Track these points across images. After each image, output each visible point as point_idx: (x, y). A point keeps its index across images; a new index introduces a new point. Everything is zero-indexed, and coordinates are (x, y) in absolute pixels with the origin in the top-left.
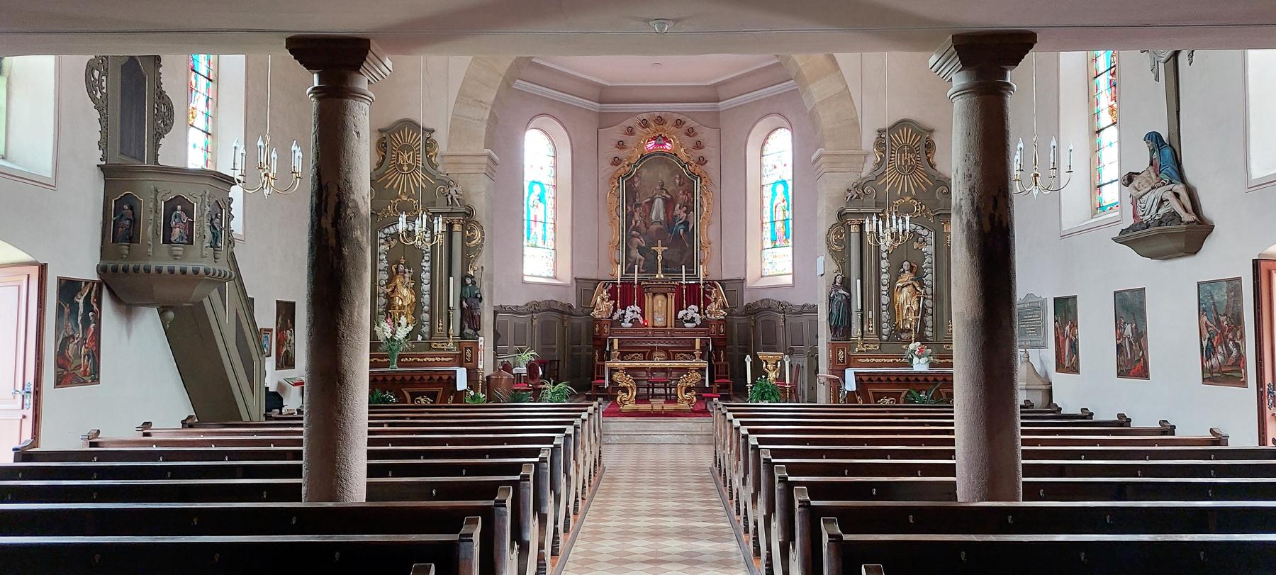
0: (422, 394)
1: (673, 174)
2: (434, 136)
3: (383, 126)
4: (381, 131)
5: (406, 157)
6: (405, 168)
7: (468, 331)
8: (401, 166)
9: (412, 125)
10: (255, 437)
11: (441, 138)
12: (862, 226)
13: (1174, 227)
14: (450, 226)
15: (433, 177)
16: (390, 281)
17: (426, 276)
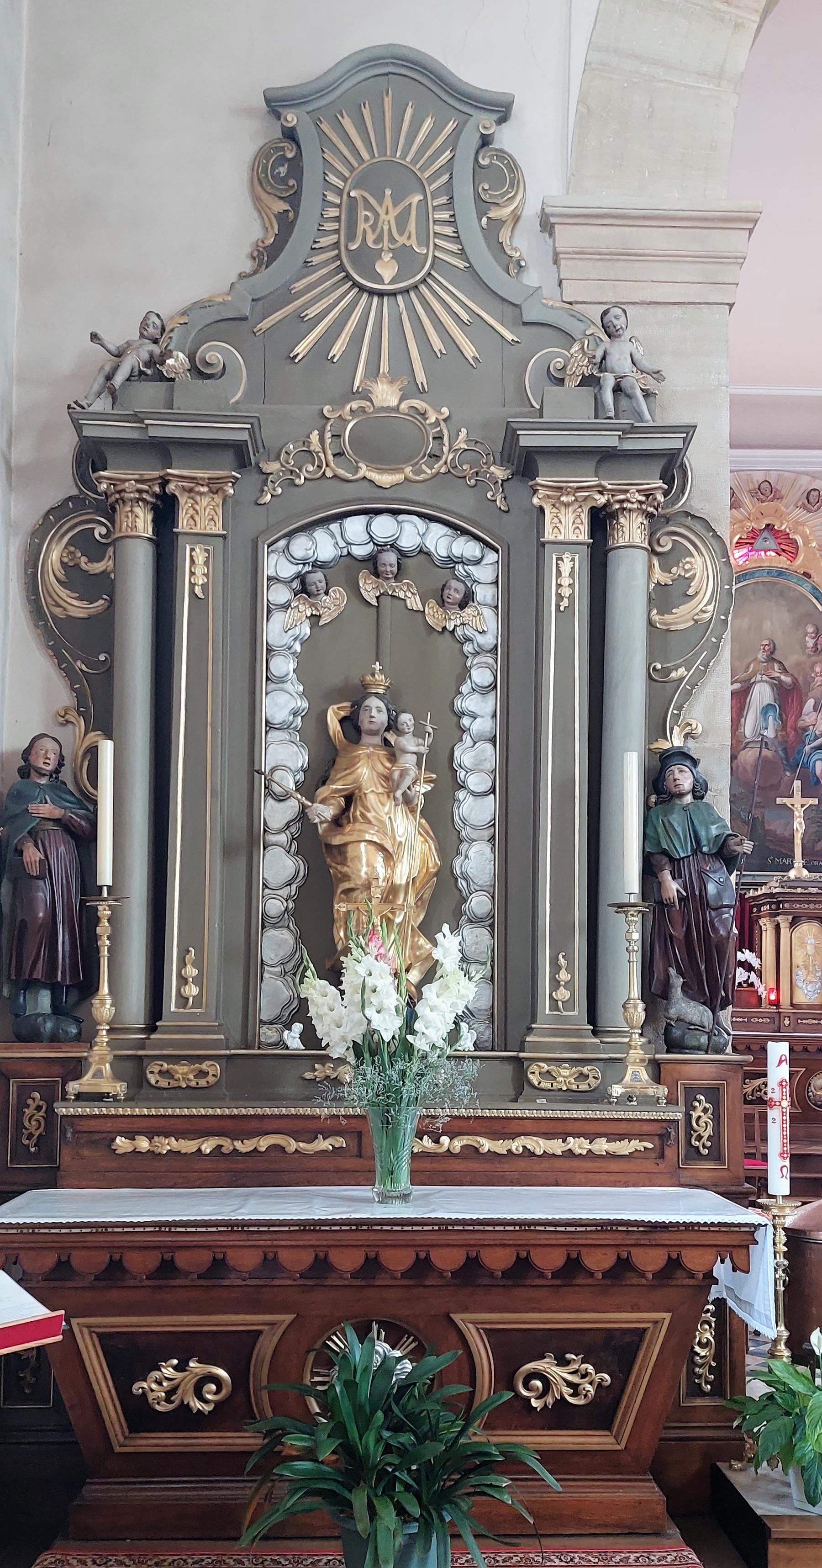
0: (560, 1344)
1: (800, 622)
2: (507, 138)
3: (288, 75)
4: (276, 104)
5: (388, 217)
6: (387, 269)
7: (687, 1009)
8: (366, 259)
9: (409, 74)
10: (162, 1486)
11: (537, 143)
12: (165, 510)
13: (425, 1514)
14: (601, 521)
15: (512, 311)
16: (315, 779)
17: (476, 760)
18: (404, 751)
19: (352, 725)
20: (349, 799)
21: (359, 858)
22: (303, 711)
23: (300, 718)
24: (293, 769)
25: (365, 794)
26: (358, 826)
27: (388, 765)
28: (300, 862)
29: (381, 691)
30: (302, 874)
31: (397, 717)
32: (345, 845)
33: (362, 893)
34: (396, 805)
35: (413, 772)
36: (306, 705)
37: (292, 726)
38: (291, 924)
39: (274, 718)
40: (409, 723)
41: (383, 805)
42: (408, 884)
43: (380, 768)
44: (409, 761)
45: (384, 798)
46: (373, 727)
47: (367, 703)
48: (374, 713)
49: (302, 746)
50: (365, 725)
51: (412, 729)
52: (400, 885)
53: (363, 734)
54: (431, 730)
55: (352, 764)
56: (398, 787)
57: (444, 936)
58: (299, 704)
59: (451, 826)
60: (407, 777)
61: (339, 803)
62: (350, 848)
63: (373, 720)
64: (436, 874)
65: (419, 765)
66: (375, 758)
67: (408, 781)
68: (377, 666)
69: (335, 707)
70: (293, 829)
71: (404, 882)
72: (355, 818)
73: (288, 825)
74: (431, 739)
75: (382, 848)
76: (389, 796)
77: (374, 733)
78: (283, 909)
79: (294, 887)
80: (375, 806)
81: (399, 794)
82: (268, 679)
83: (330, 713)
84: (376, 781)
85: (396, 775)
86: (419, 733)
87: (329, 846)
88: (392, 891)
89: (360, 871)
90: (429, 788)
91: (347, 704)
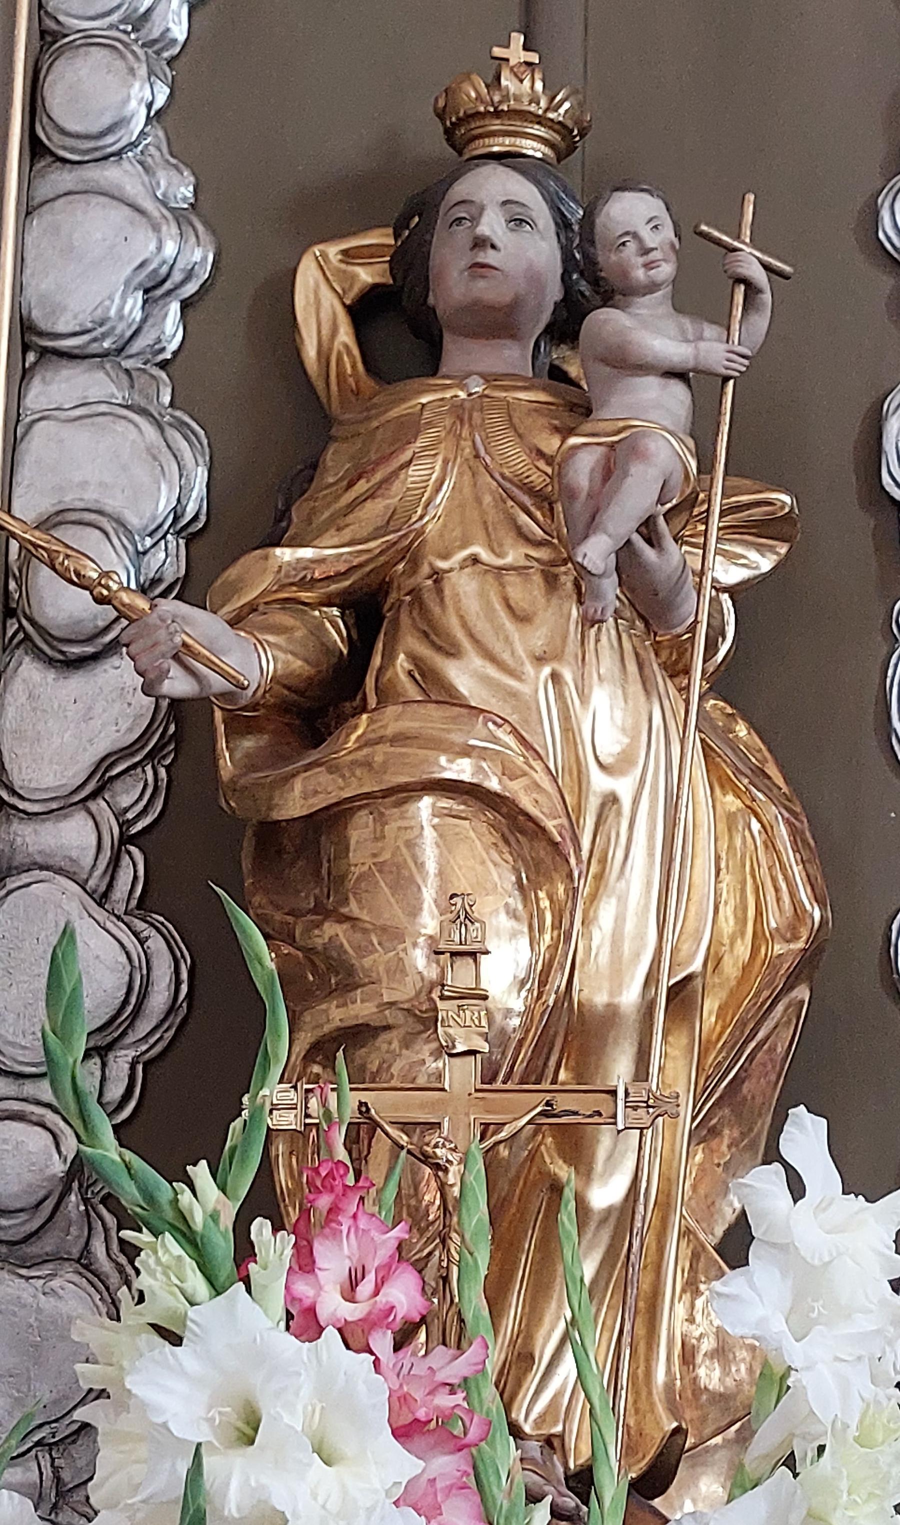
18: (627, 364)
19: (402, 324)
20: (369, 606)
21: (404, 881)
22: (189, 275)
23: (174, 308)
24: (134, 521)
25: (437, 576)
26: (393, 719)
27: (551, 444)
28: (157, 943)
29: (533, 149)
30: (159, 999)
31: (589, 220)
32: (331, 820)
33: (407, 1044)
34: (590, 621)
35: (667, 453)
36: (200, 255)
37: (137, 346)
38: (98, 1247)
39: (56, 310)
40: (651, 239)
41: (522, 618)
42: (648, 1010)
43: (515, 458)
44: (656, 410)
45: (527, 592)
46: (487, 290)
47: (461, 189)
48: (492, 224)
49: (180, 426)
50: (452, 285)
51: (666, 271)
52: (612, 1013)
53: (447, 338)
54: (760, 276)
55: (377, 460)
56: (592, 524)
57: (797, 1187)
58: (170, 249)
59: (873, 743)
60: (636, 469)
61: (317, 630)
62: (360, 830)
63: (489, 257)
64: (806, 967)
65: (701, 433)
66: (496, 418)
67: (637, 496)
68: (516, 51)
69: (333, 250)
70: (127, 795)
71: (630, 996)
72: (386, 695)
73: (102, 778)
74: (761, 322)
75: (512, 823)
76: (551, 582)
77: (497, 323)
78: (59, 1168)
79: (120, 1063)
80: (481, 627)
81: (596, 552)
82: (36, 149)
83: (308, 275)
84: (492, 516)
85: (584, 469)
86: (704, 291)
87: (270, 833)
88: (564, 1034)
89: (394, 935)
90: (766, 564)
91: (380, 237)
